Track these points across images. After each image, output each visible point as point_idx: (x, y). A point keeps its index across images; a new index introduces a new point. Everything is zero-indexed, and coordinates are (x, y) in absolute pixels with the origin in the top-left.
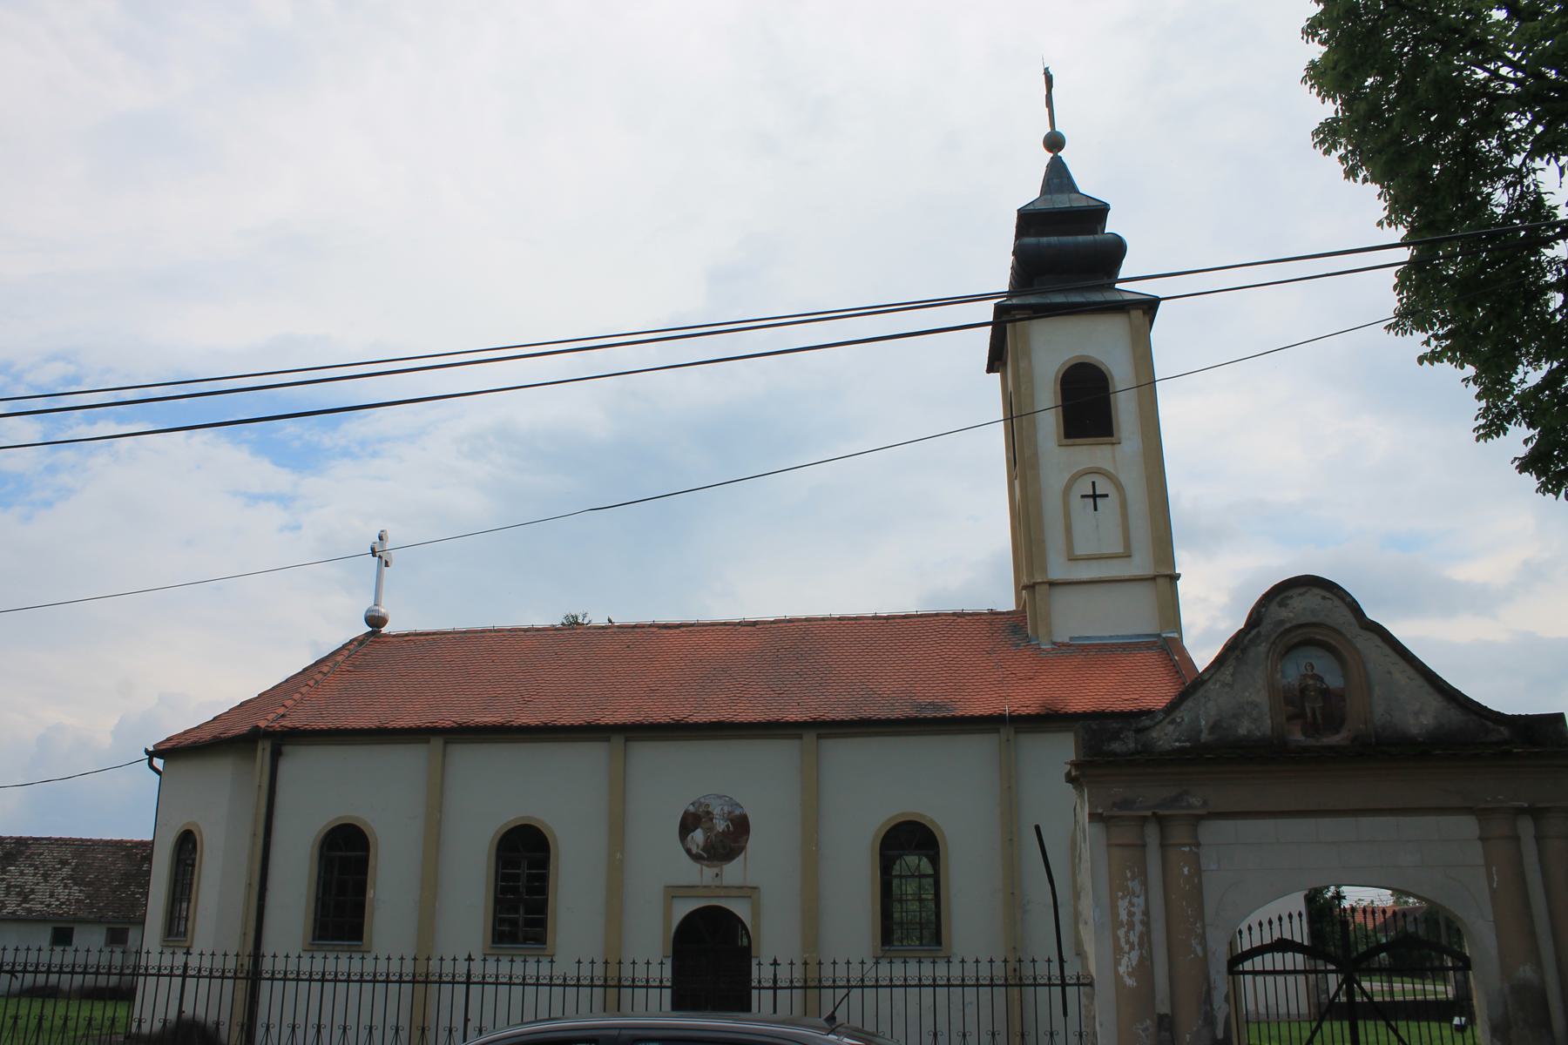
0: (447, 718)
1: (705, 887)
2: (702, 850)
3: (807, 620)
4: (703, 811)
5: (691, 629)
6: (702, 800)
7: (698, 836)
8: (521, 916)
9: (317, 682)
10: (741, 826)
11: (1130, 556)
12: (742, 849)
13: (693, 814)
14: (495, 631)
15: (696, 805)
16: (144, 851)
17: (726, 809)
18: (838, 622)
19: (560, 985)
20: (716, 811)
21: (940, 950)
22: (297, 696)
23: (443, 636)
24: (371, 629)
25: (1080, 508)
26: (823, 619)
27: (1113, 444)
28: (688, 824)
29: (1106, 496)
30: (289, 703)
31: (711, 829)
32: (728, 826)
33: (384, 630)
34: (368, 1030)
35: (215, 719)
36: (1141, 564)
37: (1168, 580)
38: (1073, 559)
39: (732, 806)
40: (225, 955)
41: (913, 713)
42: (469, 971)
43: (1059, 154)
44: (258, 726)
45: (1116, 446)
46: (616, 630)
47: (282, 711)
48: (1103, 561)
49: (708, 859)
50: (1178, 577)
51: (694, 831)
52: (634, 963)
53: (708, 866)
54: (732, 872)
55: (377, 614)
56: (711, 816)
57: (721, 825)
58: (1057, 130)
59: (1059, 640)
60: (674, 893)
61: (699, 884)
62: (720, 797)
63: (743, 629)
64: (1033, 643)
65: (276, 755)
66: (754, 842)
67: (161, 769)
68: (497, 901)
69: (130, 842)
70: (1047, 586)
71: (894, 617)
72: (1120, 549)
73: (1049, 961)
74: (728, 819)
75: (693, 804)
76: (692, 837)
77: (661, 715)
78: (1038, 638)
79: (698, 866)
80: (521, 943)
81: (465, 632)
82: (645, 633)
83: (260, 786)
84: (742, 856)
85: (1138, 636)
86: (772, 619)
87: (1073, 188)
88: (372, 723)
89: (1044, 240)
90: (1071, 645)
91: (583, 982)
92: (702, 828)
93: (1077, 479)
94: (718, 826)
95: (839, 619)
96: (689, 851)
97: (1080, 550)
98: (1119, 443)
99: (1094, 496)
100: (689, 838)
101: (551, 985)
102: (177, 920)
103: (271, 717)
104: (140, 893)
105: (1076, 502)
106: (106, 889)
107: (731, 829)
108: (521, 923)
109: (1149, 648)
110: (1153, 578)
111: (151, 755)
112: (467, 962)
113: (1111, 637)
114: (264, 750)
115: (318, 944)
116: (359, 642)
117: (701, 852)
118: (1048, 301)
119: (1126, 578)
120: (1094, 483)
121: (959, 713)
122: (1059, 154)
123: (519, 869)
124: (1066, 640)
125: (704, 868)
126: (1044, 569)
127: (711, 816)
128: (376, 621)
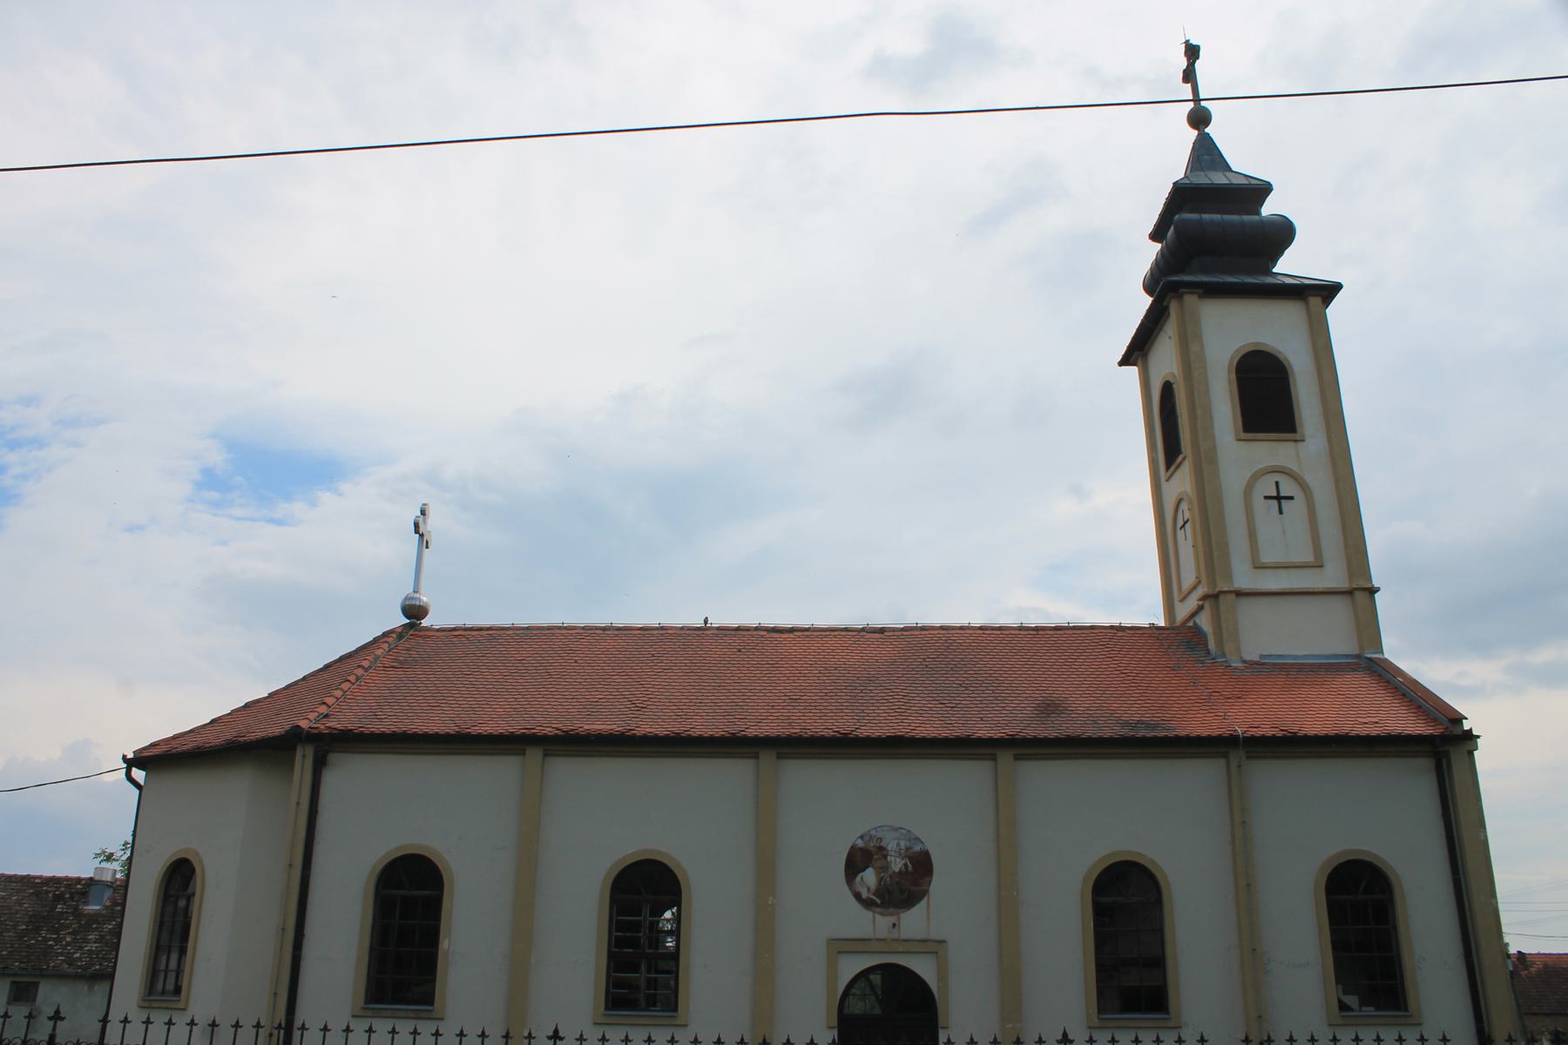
0: (548, 725)
1: (879, 940)
2: (874, 894)
3: (942, 628)
4: (874, 846)
5: (806, 633)
6: (873, 833)
7: (869, 877)
9: (358, 679)
10: (921, 865)
11: (1322, 566)
13: (861, 849)
14: (566, 628)
15: (867, 838)
16: (58, 888)
17: (903, 844)
18: (981, 632)
20: (891, 846)
22: (338, 693)
23: (502, 632)
24: (408, 621)
25: (1265, 512)
26: (962, 628)
27: (1296, 441)
28: (856, 862)
29: (1291, 498)
30: (330, 701)
31: (885, 868)
32: (906, 865)
33: (425, 623)
35: (213, 721)
36: (1333, 575)
37: (1367, 593)
38: (1259, 566)
39: (909, 840)
40: (237, 1026)
41: (1126, 732)
43: (1207, 130)
44: (298, 726)
45: (1300, 444)
46: (716, 632)
47: (323, 709)
50: (1373, 591)
51: (863, 870)
53: (882, 914)
54: (913, 922)
55: (418, 603)
56: (885, 853)
57: (897, 864)
59: (1247, 658)
60: (841, 947)
61: (872, 937)
62: (896, 829)
63: (868, 636)
65: (320, 764)
66: (937, 884)
67: (142, 783)
68: (611, 955)
69: (40, 877)
72: (1309, 558)
74: (906, 856)
75: (862, 837)
76: (862, 878)
78: (1224, 655)
79: (870, 914)
80: (643, 1010)
81: (527, 628)
83: (298, 803)
84: (924, 902)
85: (1327, 657)
86: (902, 626)
87: (1227, 167)
88: (450, 728)
89: (1206, 217)
90: (1263, 664)
92: (873, 867)
93: (1259, 478)
94: (893, 865)
96: (857, 896)
97: (1266, 558)
98: (1303, 441)
99: (1278, 498)
100: (858, 879)
102: (162, 974)
103: (312, 716)
104: (54, 940)
106: (11, 934)
109: (1353, 670)
111: (130, 763)
113: (1305, 656)
114: (303, 759)
115: (373, 1009)
116: (400, 634)
117: (874, 898)
118: (1222, 280)
119: (1320, 590)
120: (1277, 483)
121: (1171, 734)
122: (1207, 130)
123: (641, 916)
124: (1256, 658)
125: (877, 915)
126: (1229, 576)
127: (885, 853)
128: (414, 612)
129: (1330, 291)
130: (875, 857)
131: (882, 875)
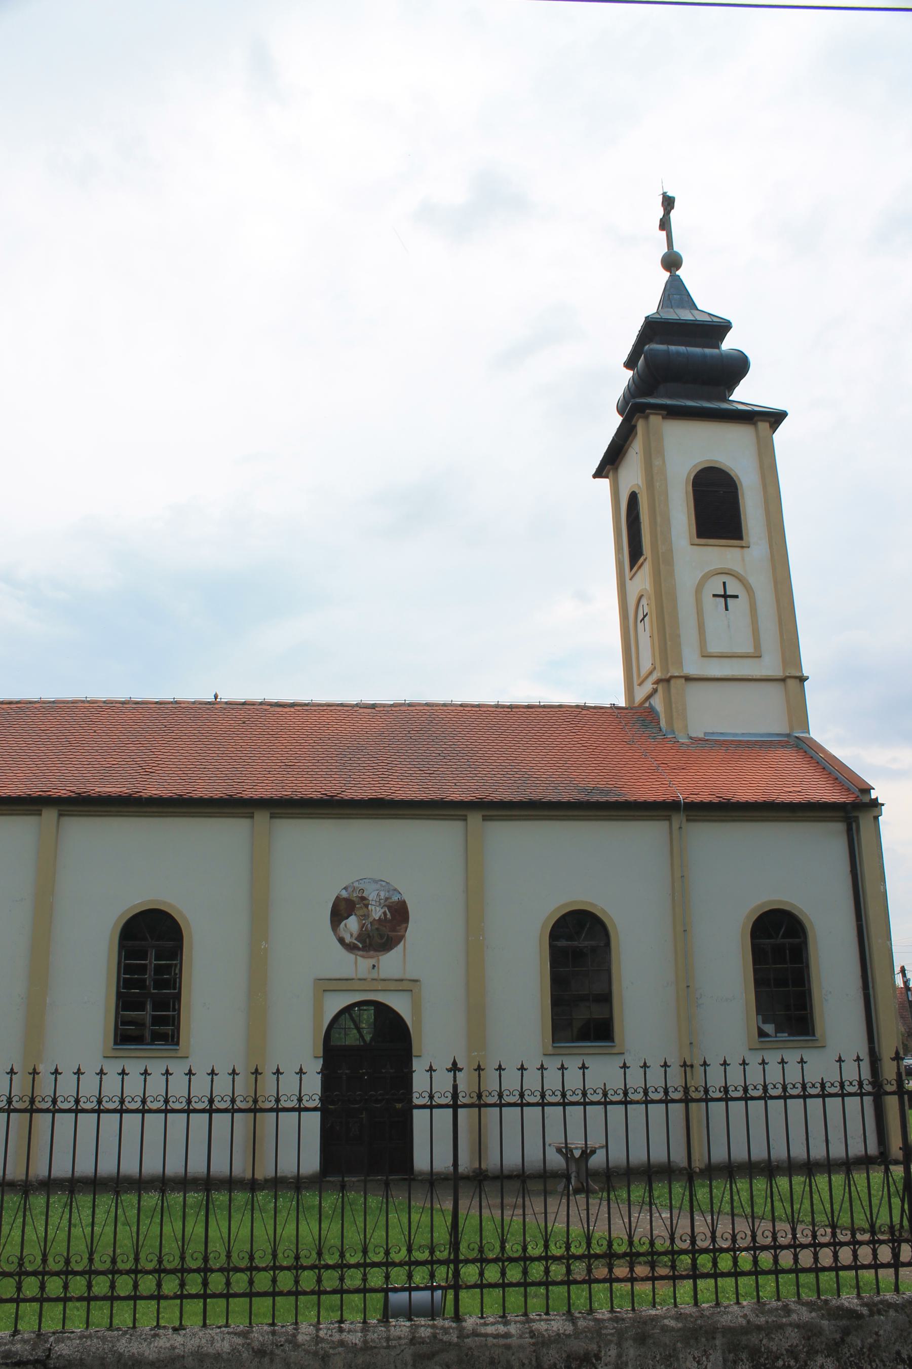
2: (356, 939)
3: (427, 705)
6: (356, 884)
7: (352, 924)
8: (148, 1013)
12: (400, 938)
13: (345, 899)
14: (88, 702)
15: (350, 890)
17: (382, 894)
19: (598, 1103)
20: (372, 896)
21: (614, 1046)
25: (713, 607)
26: (444, 705)
27: (742, 547)
29: (736, 597)
31: (366, 916)
32: (385, 913)
34: (718, 1234)
36: (770, 666)
37: (798, 680)
38: (706, 655)
39: (388, 892)
41: (582, 797)
42: (455, 1087)
46: (225, 706)
48: (734, 659)
49: (363, 949)
51: (347, 918)
52: (500, 1068)
53: (362, 956)
56: (365, 902)
57: (377, 912)
58: (675, 249)
61: (354, 976)
62: (376, 882)
63: (361, 711)
64: (668, 737)
66: (413, 931)
70: (683, 680)
71: (517, 707)
72: (750, 649)
73: (858, 1059)
75: (346, 888)
76: (346, 925)
77: (312, 791)
81: (54, 702)
82: (257, 710)
84: (400, 946)
89: (673, 348)
90: (707, 740)
91: (549, 1099)
92: (355, 915)
95: (461, 705)
96: (341, 941)
97: (713, 648)
98: (749, 547)
99: (725, 596)
100: (342, 925)
101: (585, 1104)
105: (708, 600)
107: (389, 916)
108: (148, 1021)
110: (783, 680)
112: (477, 1072)
117: (356, 942)
120: (724, 583)
122: (678, 273)
124: (701, 735)
126: (680, 664)
129: (776, 418)
130: (357, 906)
131: (364, 922)
